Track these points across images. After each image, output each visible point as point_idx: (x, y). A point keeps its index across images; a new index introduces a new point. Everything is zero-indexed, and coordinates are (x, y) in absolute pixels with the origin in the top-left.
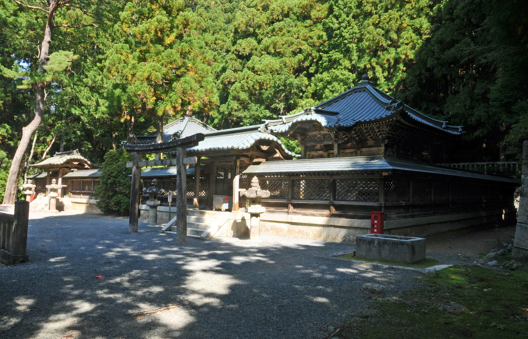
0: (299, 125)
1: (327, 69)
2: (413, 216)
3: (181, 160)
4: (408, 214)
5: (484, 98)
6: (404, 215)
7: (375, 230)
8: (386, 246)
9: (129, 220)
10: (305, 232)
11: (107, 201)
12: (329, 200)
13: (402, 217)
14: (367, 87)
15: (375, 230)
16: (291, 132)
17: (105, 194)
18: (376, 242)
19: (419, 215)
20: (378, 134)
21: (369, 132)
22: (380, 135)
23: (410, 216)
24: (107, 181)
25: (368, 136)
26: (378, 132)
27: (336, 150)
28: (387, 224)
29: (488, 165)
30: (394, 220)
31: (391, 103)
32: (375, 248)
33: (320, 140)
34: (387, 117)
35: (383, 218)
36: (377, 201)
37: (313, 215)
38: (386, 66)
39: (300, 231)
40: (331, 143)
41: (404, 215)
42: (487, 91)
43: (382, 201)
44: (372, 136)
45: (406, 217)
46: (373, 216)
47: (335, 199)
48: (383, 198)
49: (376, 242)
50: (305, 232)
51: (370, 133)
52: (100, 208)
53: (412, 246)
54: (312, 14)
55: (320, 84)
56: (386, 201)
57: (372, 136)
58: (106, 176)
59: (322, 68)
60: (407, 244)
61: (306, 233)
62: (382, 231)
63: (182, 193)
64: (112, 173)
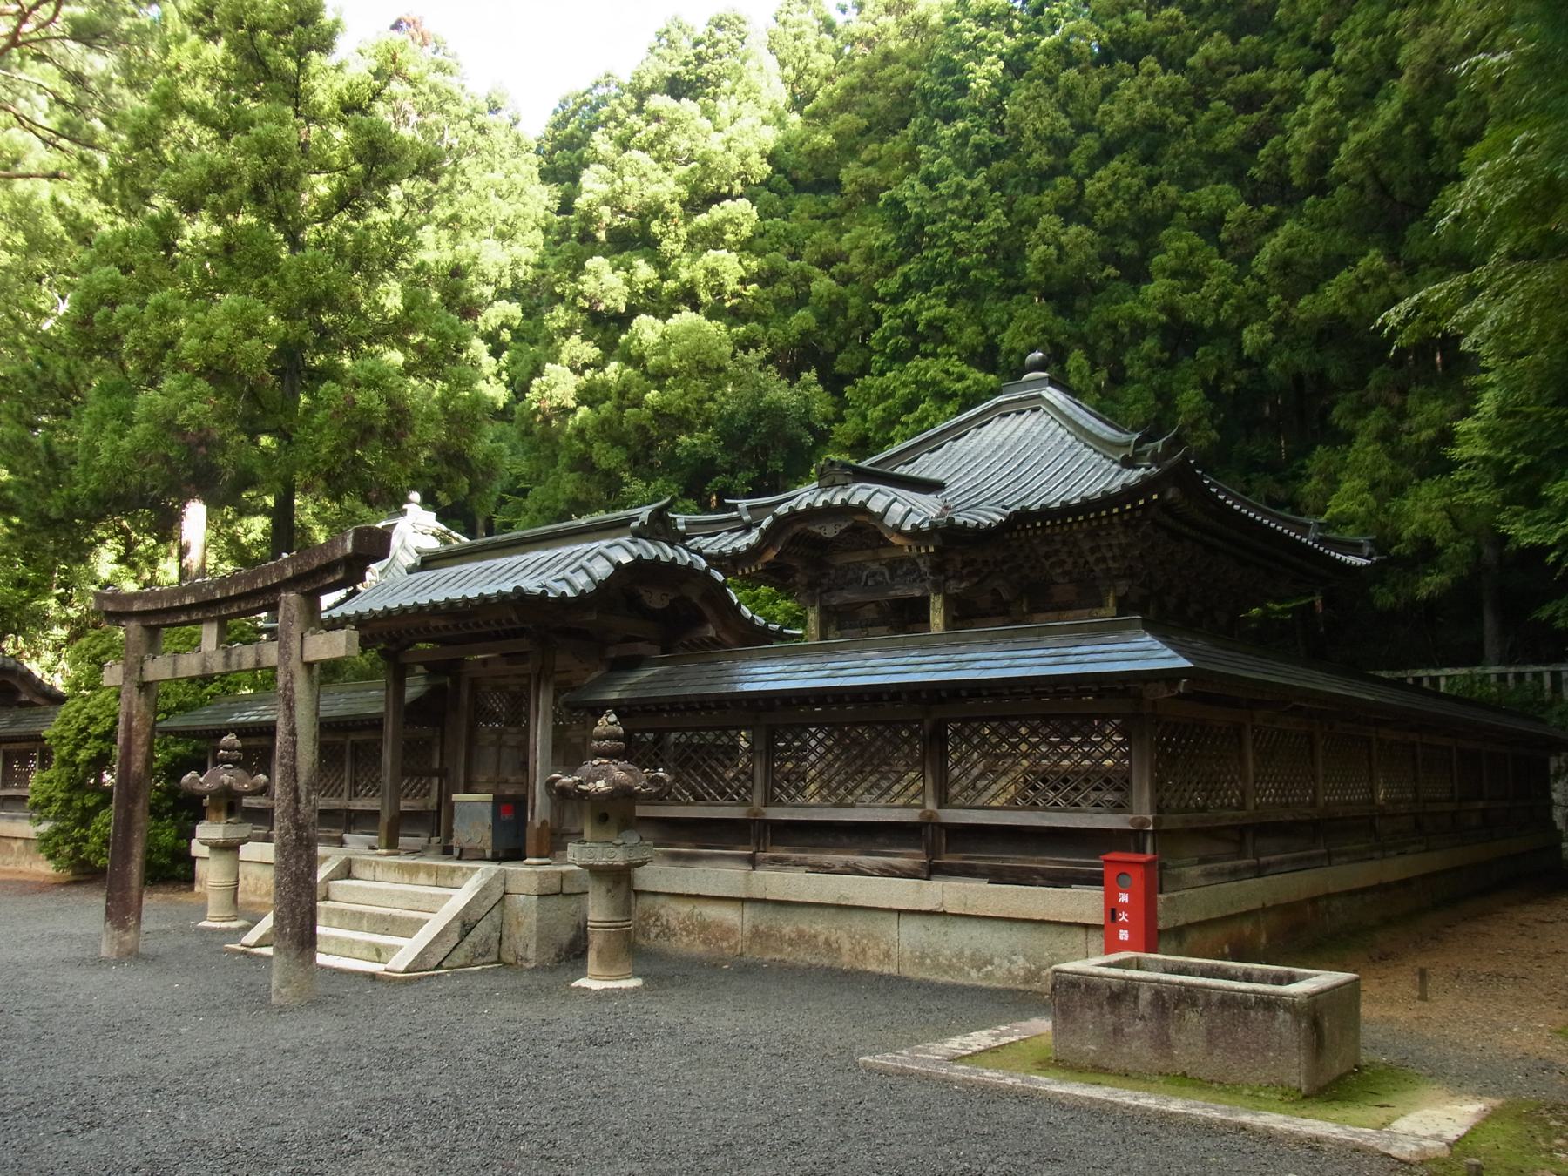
0: (797, 528)
1: (900, 357)
2: (1259, 871)
3: (295, 645)
4: (1241, 863)
5: (1434, 460)
6: (1229, 864)
7: (1124, 935)
8: (1192, 1016)
9: (103, 901)
10: (822, 938)
11: (76, 833)
12: (922, 806)
13: (1221, 873)
14: (1044, 394)
15: (1124, 935)
16: (771, 555)
17: (67, 803)
18: (1145, 996)
19: (1282, 862)
20: (1091, 559)
21: (1057, 551)
22: (1098, 561)
23: (1250, 868)
24: (72, 754)
25: (1053, 566)
26: (1092, 551)
27: (937, 619)
28: (1175, 907)
29: (1502, 678)
30: (1198, 895)
31: (1139, 443)
32: (1140, 1025)
33: (877, 584)
34: (1128, 492)
35: (1157, 880)
36: (1119, 807)
37: (856, 871)
38: (1105, 344)
39: (801, 934)
40: (917, 593)
41: (1229, 864)
42: (1447, 437)
43: (1142, 811)
44: (1068, 566)
45: (1235, 874)
46: (1109, 874)
47: (943, 801)
48: (1147, 796)
49: (1145, 996)
50: (822, 938)
51: (1063, 556)
52: (51, 857)
53: (1314, 1012)
54: (845, 176)
55: (876, 413)
56: (1159, 808)
57: (1068, 566)
58: (70, 734)
59: (882, 353)
60: (1289, 1005)
61: (827, 942)
62: (1152, 939)
63: (296, 790)
64: (92, 720)
